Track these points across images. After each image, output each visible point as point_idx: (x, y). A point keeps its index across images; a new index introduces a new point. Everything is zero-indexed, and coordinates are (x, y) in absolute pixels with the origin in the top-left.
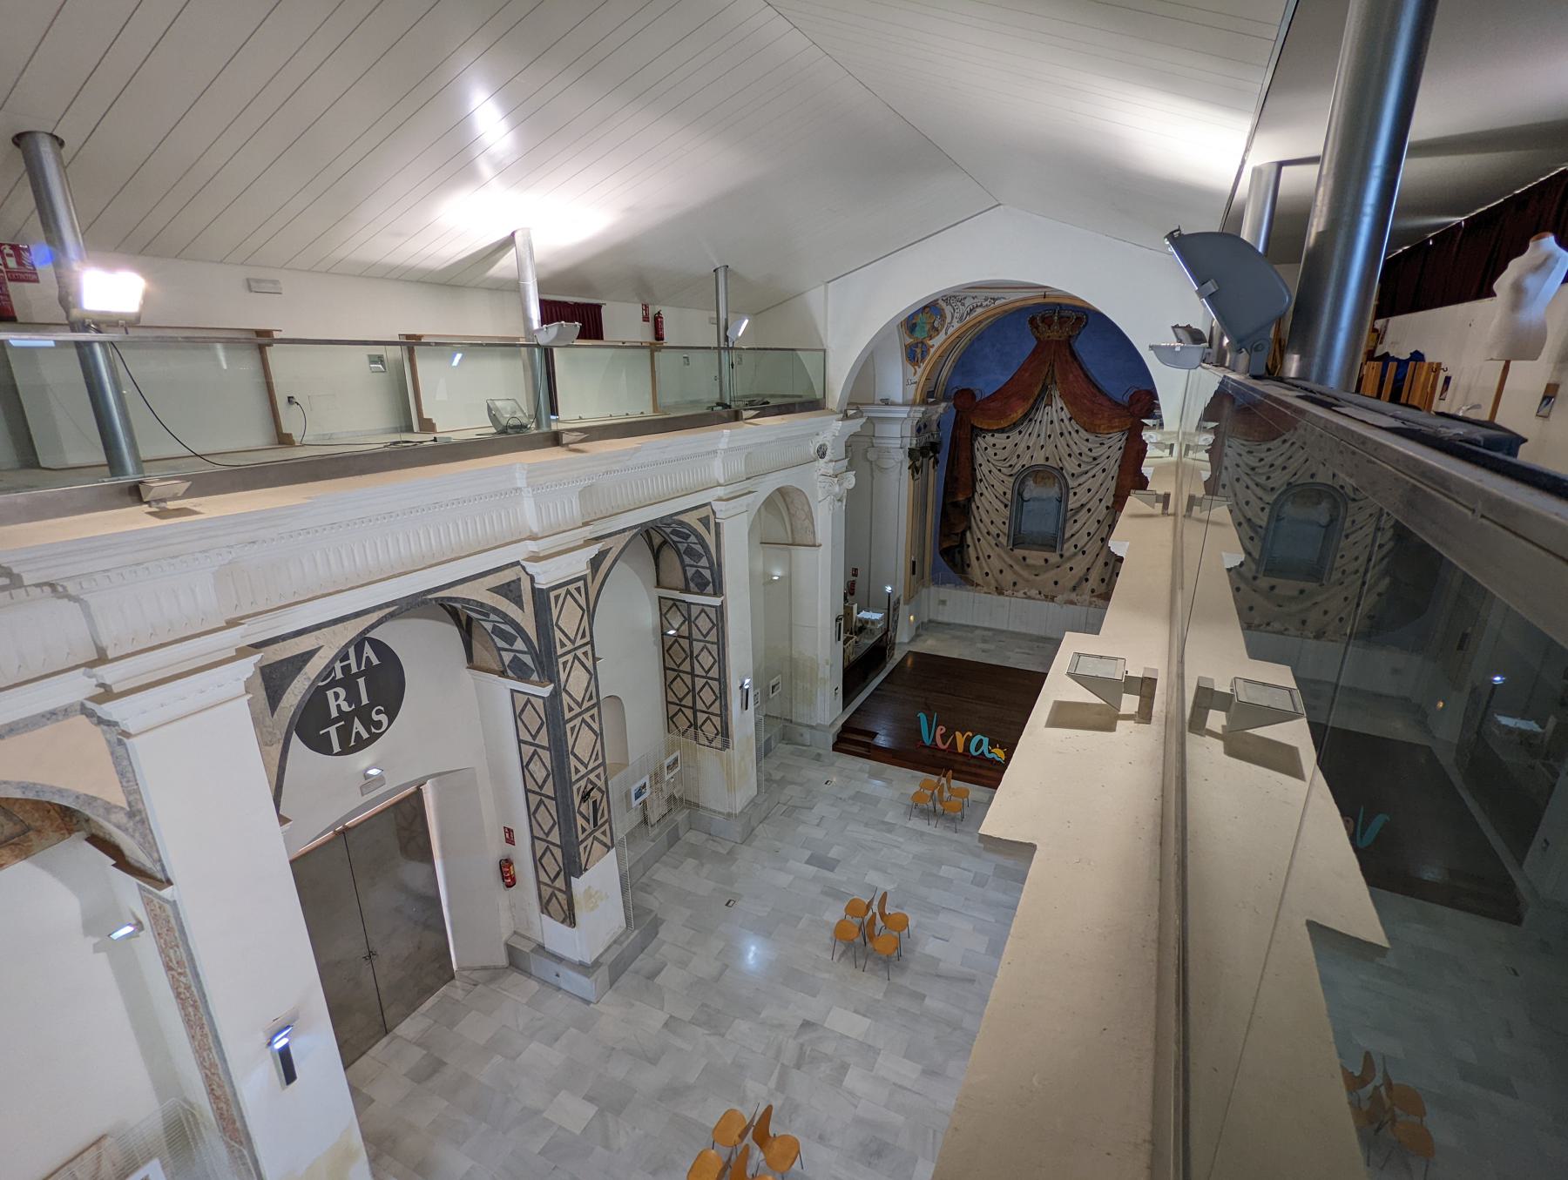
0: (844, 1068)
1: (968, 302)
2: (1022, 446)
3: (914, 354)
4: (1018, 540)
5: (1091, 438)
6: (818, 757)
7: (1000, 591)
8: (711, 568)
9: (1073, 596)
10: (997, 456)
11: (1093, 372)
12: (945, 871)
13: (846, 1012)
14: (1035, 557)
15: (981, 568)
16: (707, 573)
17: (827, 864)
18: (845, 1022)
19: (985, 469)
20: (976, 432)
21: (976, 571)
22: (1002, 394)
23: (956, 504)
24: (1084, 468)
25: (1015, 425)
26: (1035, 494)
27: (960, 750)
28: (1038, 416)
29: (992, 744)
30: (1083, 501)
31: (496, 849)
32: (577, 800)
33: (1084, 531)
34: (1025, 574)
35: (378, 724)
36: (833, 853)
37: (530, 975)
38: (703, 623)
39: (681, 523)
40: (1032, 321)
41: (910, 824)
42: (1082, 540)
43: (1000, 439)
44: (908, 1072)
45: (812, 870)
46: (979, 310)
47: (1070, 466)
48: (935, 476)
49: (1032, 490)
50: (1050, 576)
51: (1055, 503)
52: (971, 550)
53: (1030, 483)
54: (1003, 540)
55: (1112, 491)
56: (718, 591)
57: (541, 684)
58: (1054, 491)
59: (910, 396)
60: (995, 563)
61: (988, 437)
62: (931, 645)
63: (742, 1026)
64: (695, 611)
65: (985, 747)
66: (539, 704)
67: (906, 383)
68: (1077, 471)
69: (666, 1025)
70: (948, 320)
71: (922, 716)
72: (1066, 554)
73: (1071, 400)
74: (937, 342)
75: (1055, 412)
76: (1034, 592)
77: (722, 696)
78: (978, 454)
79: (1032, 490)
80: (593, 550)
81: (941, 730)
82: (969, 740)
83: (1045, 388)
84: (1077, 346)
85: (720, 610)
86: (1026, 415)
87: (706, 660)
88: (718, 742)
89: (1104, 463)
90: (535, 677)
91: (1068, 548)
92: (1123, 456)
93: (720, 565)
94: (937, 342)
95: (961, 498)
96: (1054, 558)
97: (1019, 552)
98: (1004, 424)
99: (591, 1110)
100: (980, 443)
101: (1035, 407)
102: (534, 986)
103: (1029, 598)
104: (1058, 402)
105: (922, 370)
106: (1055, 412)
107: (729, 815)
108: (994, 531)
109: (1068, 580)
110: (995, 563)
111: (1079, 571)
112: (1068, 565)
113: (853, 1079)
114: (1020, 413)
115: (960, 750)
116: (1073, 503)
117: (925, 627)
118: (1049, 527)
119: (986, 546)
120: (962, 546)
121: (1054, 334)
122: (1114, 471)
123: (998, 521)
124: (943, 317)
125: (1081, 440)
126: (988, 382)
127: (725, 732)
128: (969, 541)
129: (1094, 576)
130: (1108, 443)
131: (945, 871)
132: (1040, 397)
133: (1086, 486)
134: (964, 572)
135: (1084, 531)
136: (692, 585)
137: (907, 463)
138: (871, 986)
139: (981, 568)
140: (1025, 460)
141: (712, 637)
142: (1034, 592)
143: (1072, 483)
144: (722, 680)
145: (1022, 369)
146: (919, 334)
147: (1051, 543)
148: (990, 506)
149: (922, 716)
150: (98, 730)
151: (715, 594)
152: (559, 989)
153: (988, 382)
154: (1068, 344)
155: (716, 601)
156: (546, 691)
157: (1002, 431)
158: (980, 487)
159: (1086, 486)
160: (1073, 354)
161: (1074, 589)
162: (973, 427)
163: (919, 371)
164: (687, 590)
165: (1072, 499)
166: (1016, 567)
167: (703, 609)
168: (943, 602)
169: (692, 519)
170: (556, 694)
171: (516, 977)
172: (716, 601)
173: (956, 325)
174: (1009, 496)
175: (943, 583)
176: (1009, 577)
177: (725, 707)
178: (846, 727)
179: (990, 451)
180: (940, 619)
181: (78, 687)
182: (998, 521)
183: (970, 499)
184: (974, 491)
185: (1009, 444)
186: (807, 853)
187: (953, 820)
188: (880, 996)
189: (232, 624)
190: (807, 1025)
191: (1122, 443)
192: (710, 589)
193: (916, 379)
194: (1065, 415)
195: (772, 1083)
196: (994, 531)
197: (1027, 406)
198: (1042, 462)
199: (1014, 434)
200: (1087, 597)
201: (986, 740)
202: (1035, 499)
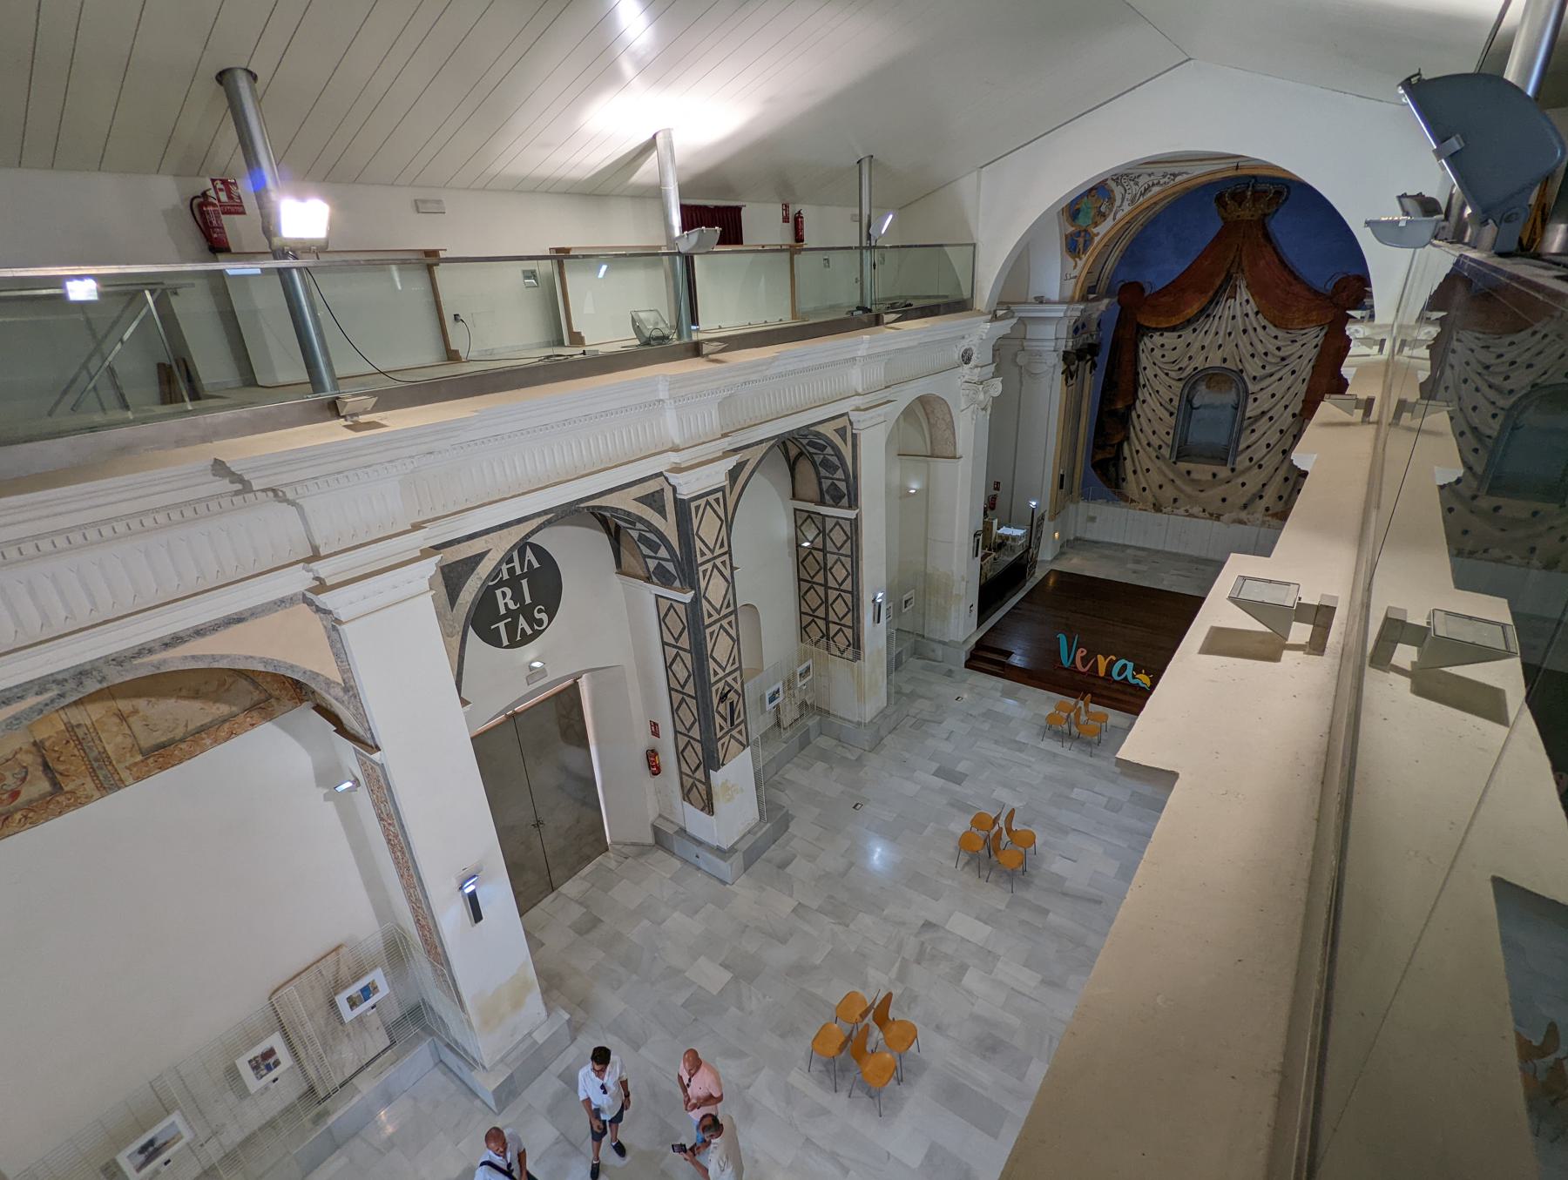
0: (963, 968)
1: (1143, 181)
2: (1197, 345)
3: (1074, 246)
4: (1183, 452)
5: (1280, 334)
6: (950, 673)
7: (1157, 508)
8: (846, 480)
9: (1243, 515)
10: (1164, 358)
12: (1077, 793)
13: (967, 916)
14: (1202, 471)
15: (1138, 483)
16: (842, 486)
17: (958, 778)
18: (965, 927)
19: (1150, 373)
20: (1142, 331)
21: (1131, 486)
22: (1177, 287)
23: (1114, 413)
24: (1269, 370)
25: (1189, 322)
26: (1207, 400)
27: (1102, 672)
28: (1219, 311)
29: (1137, 670)
30: (1265, 408)
31: (644, 740)
32: (715, 701)
33: (1263, 442)
34: (1188, 489)
35: (540, 622)
36: (962, 767)
37: (673, 854)
38: (837, 535)
39: (818, 434)
40: (1220, 199)
41: (1042, 745)
42: (1259, 452)
43: (1169, 339)
44: (1028, 980)
45: (939, 782)
46: (1156, 189)
47: (1252, 368)
48: (1091, 382)
49: (1203, 396)
50: (1218, 492)
51: (1230, 410)
52: (1128, 463)
53: (1202, 387)
54: (1166, 452)
55: (1302, 396)
56: (853, 503)
57: (682, 590)
58: (1230, 397)
59: (1068, 293)
60: (1155, 477)
61: (1156, 336)
62: (1076, 564)
63: (866, 920)
64: (829, 524)
65: (1129, 673)
66: (681, 609)
67: (1065, 278)
68: (1260, 373)
69: (794, 910)
70: (1118, 203)
71: (1062, 638)
72: (1239, 468)
73: (1258, 290)
74: (1103, 229)
75: (1240, 305)
77: (855, 608)
78: (1142, 356)
79: (1203, 396)
80: (731, 462)
81: (1082, 652)
82: (1111, 664)
83: (1229, 277)
84: (1273, 226)
85: (855, 524)
86: (1202, 311)
87: (840, 572)
88: (849, 654)
89: (1294, 363)
90: (677, 583)
91: (1242, 461)
92: (1319, 355)
93: (855, 477)
94: (1103, 229)
95: (1120, 406)
96: (1224, 472)
97: (1183, 466)
98: (1175, 321)
99: (727, 976)
100: (1146, 343)
101: (1214, 301)
102: (677, 864)
103: (1191, 515)
105: (1085, 261)
107: (859, 724)
108: (1156, 441)
109: (1238, 496)
110: (1155, 477)
111: (1252, 487)
112: (1240, 480)
113: (971, 979)
115: (1102, 672)
116: (1252, 410)
117: (1071, 545)
118: (1220, 437)
119: (1145, 459)
120: (1118, 458)
121: (1246, 213)
123: (1162, 431)
124: (1111, 200)
125: (1268, 338)
126: (1160, 273)
127: (856, 643)
131: (1077, 793)
133: (1270, 391)
134: (1117, 486)
135: (1263, 442)
136: (827, 497)
137: (1061, 367)
138: (995, 896)
139: (1138, 483)
140: (1199, 362)
141: (846, 550)
142: (1196, 510)
143: (1252, 387)
144: (855, 593)
145: (1202, 256)
146: (1083, 221)
147: (1221, 456)
148: (1153, 415)
149: (1062, 638)
150: (317, 616)
151: (850, 507)
152: (699, 869)
153: (1155, 278)
154: (1262, 224)
155: (851, 514)
156: (687, 597)
157: (1173, 329)
159: (1270, 391)
160: (1267, 236)
161: (1245, 506)
162: (1139, 326)
163: (1080, 263)
164: (822, 503)
165: (1251, 405)
166: (1178, 482)
167: (838, 522)
168: (1093, 519)
169: (828, 430)
170: (696, 601)
171: (660, 854)
172: (851, 514)
173: (1127, 208)
174: (1176, 403)
175: (1094, 499)
176: (1169, 492)
177: (857, 620)
178: (980, 645)
180: (1088, 536)
181: (323, 569)
183: (1131, 407)
184: (1135, 397)
185: (1181, 343)
186: (934, 766)
187: (1089, 744)
188: (1002, 907)
189: (417, 527)
190: (928, 925)
191: (1320, 340)
192: (845, 501)
193: (1076, 272)
194: (1251, 308)
195: (894, 973)
196: (1156, 441)
197: (1204, 300)
198: (1218, 363)
199: (1187, 334)
200: (1259, 515)
201: (1130, 665)
202: (1206, 406)
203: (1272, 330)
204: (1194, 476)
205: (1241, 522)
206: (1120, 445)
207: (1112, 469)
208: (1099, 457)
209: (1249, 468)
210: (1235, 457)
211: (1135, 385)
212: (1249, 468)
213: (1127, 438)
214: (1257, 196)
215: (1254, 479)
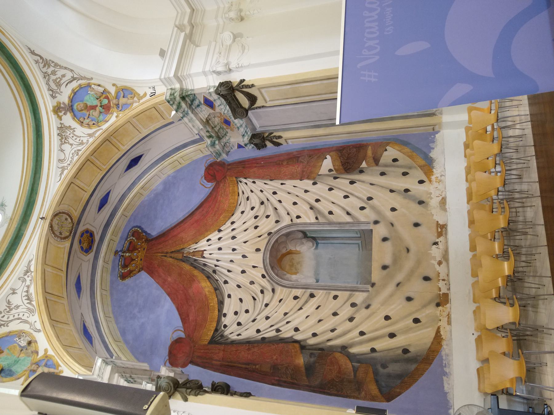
1: (16, 300)
5: (241, 209)
9: (434, 202)
10: (251, 311)
11: (180, 215)
15: (407, 330)
19: (263, 325)
20: (218, 339)
21: (418, 339)
24: (271, 212)
25: (217, 289)
30: (307, 207)
33: (344, 203)
40: (123, 277)
42: (353, 204)
43: (230, 307)
47: (266, 226)
50: (407, 234)
52: (379, 345)
54: (359, 298)
55: (297, 182)
58: (306, 250)
61: (225, 321)
68: (273, 218)
72: (373, 217)
73: (202, 232)
75: (213, 248)
76: (436, 252)
83: (185, 260)
86: (209, 277)
96: (380, 231)
97: (376, 275)
98: (214, 303)
100: (232, 332)
101: (202, 268)
104: (202, 245)
106: (213, 248)
108: (346, 311)
110: (397, 308)
112: (389, 214)
114: (206, 286)
116: (308, 218)
119: (371, 323)
120: (371, 362)
122: (275, 184)
123: (333, 305)
124: (20, 334)
125: (242, 219)
128: (364, 349)
129: (401, 184)
130: (248, 193)
132: (195, 265)
135: (344, 203)
139: (407, 330)
140: (256, 275)
142: (436, 252)
143: (286, 221)
147: (365, 238)
157: (221, 303)
158: (287, 332)
162: (213, 341)
166: (399, 278)
173: (35, 318)
176: (416, 287)
179: (243, 318)
182: (333, 305)
183: (302, 346)
185: (236, 294)
191: (249, 181)
194: (214, 236)
196: (346, 311)
198: (260, 255)
203: (238, 214)
204: (388, 261)
205: (443, 202)
206: (352, 357)
207: (394, 368)
208: (373, 389)
209: (373, 208)
210: (359, 223)
211: (279, 342)
212: (373, 208)
213: (344, 348)
214: (132, 248)
215: (384, 201)
